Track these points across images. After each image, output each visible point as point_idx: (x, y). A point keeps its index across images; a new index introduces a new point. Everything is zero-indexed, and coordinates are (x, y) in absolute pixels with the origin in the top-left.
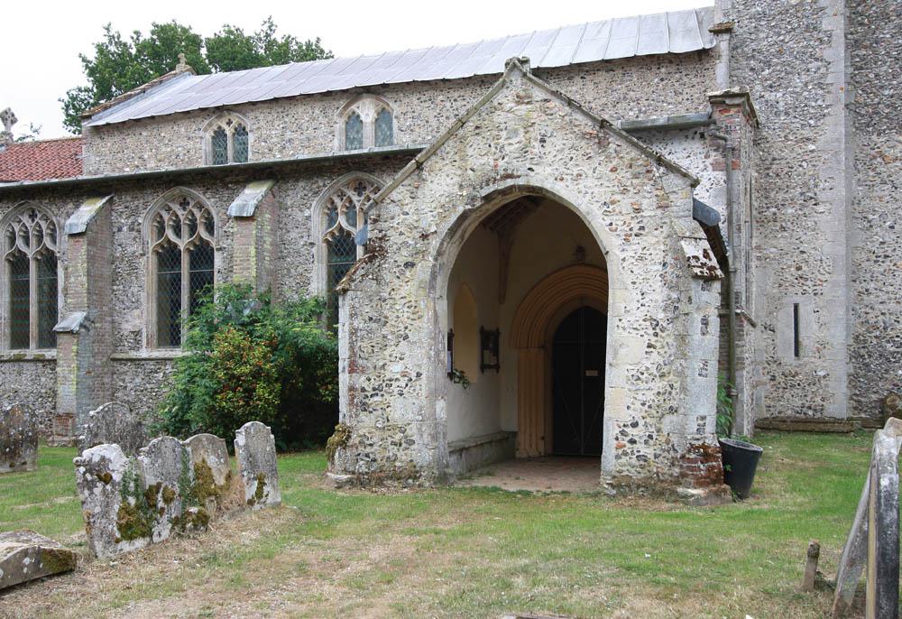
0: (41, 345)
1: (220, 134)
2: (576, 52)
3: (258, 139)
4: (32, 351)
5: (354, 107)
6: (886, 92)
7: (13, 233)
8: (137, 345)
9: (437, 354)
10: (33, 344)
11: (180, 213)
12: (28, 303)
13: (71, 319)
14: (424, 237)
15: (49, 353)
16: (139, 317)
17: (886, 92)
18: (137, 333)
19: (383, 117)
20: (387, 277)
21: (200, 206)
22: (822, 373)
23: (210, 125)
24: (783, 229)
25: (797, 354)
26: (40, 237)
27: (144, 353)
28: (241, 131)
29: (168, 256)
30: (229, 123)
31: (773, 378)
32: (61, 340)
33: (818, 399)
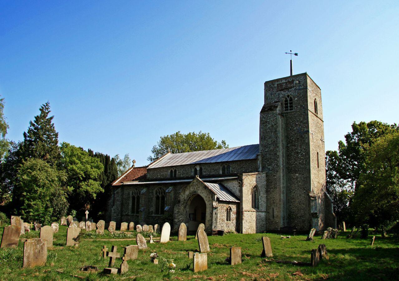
0: (161, 214)
1: (172, 171)
2: (310, 111)
3: (178, 172)
4: (135, 214)
5: (196, 167)
6: (293, 165)
7: (133, 192)
8: (152, 214)
9: (187, 217)
10: (135, 213)
11: (160, 190)
12: (135, 201)
13: (142, 209)
14: (185, 200)
15: (138, 215)
16: (153, 209)
17: (293, 165)
18: (152, 212)
19: (201, 169)
20: (180, 205)
21: (163, 189)
22: (277, 222)
23: (170, 169)
24: (271, 193)
25: (273, 218)
26: (137, 193)
27: (153, 215)
28: (175, 171)
29: (158, 198)
30: (173, 169)
31: (269, 222)
32: (140, 212)
33: (277, 227)
